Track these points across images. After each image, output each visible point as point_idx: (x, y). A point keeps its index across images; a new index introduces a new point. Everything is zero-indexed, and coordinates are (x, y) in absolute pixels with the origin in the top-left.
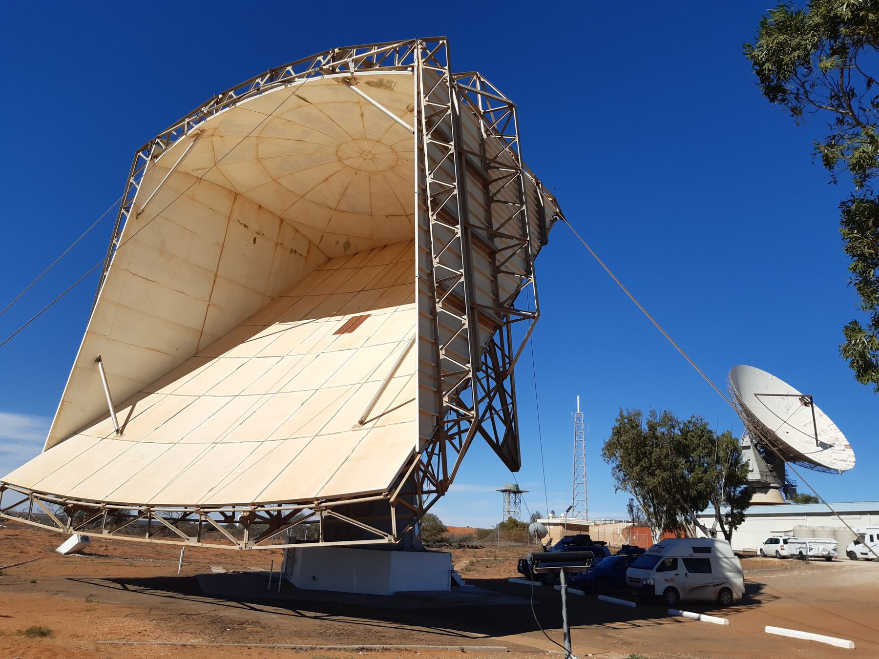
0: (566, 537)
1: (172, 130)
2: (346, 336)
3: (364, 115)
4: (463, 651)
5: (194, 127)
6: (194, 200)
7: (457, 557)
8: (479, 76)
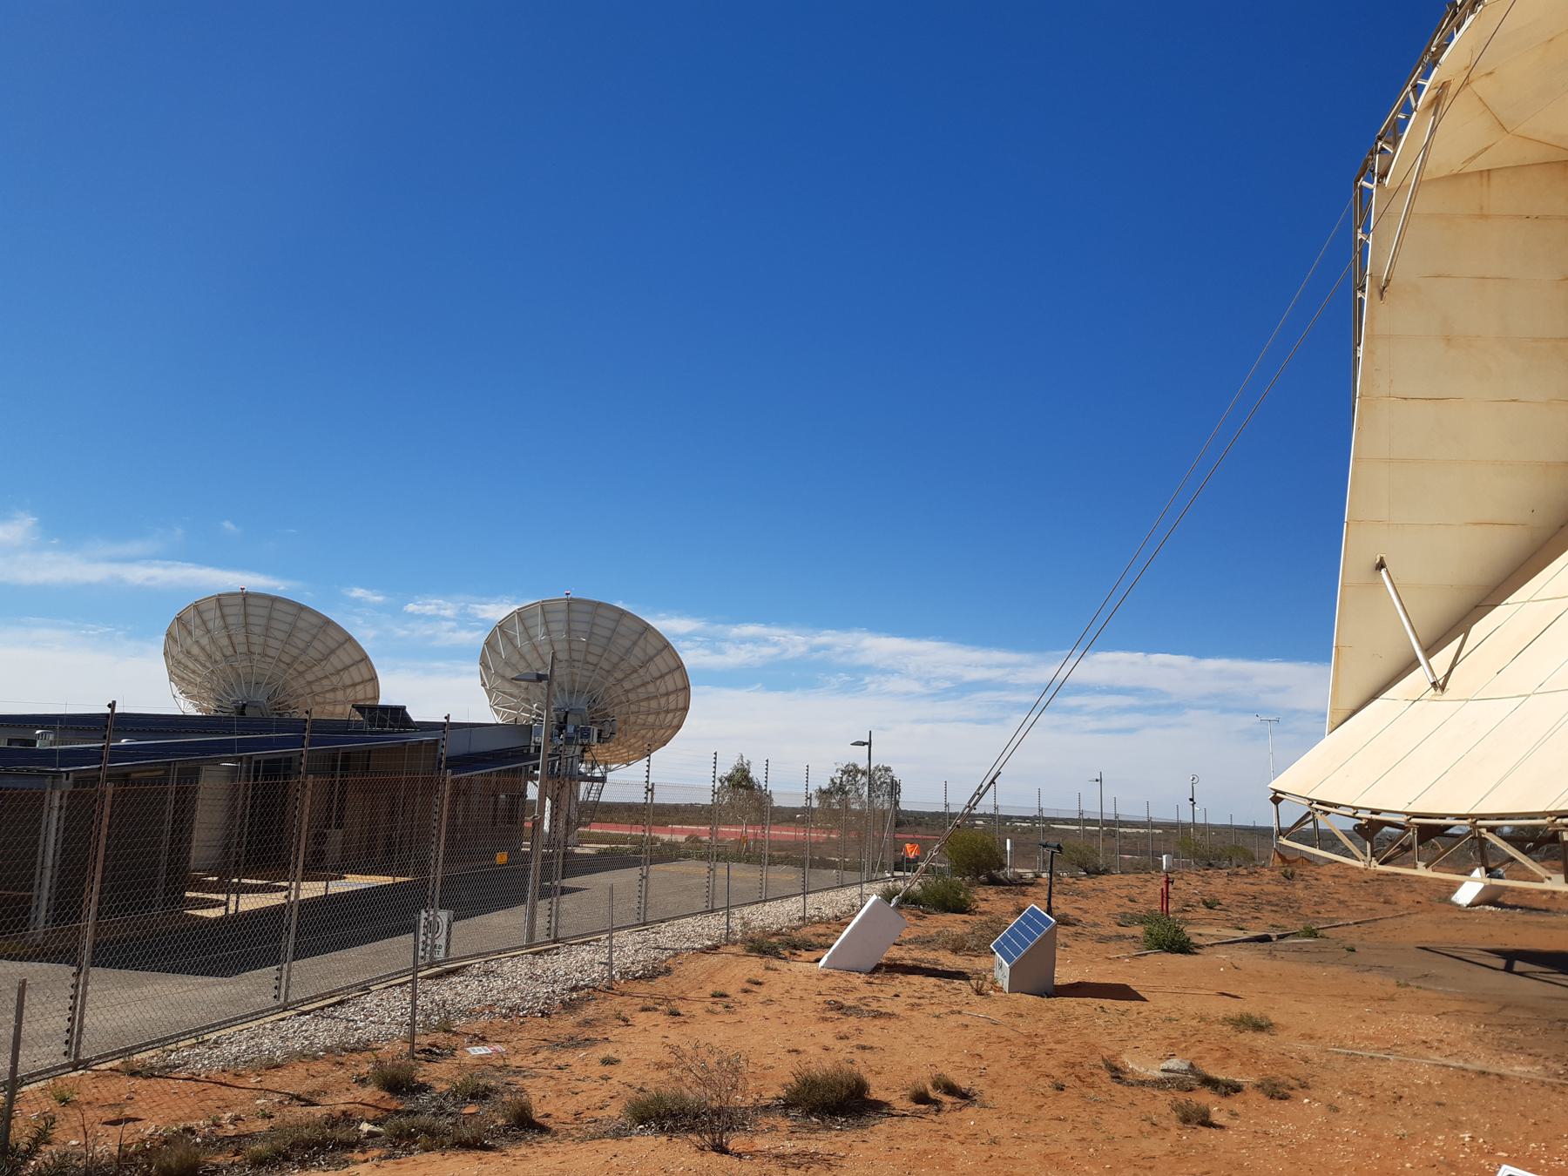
1: (1394, 113)
6: (1483, 216)
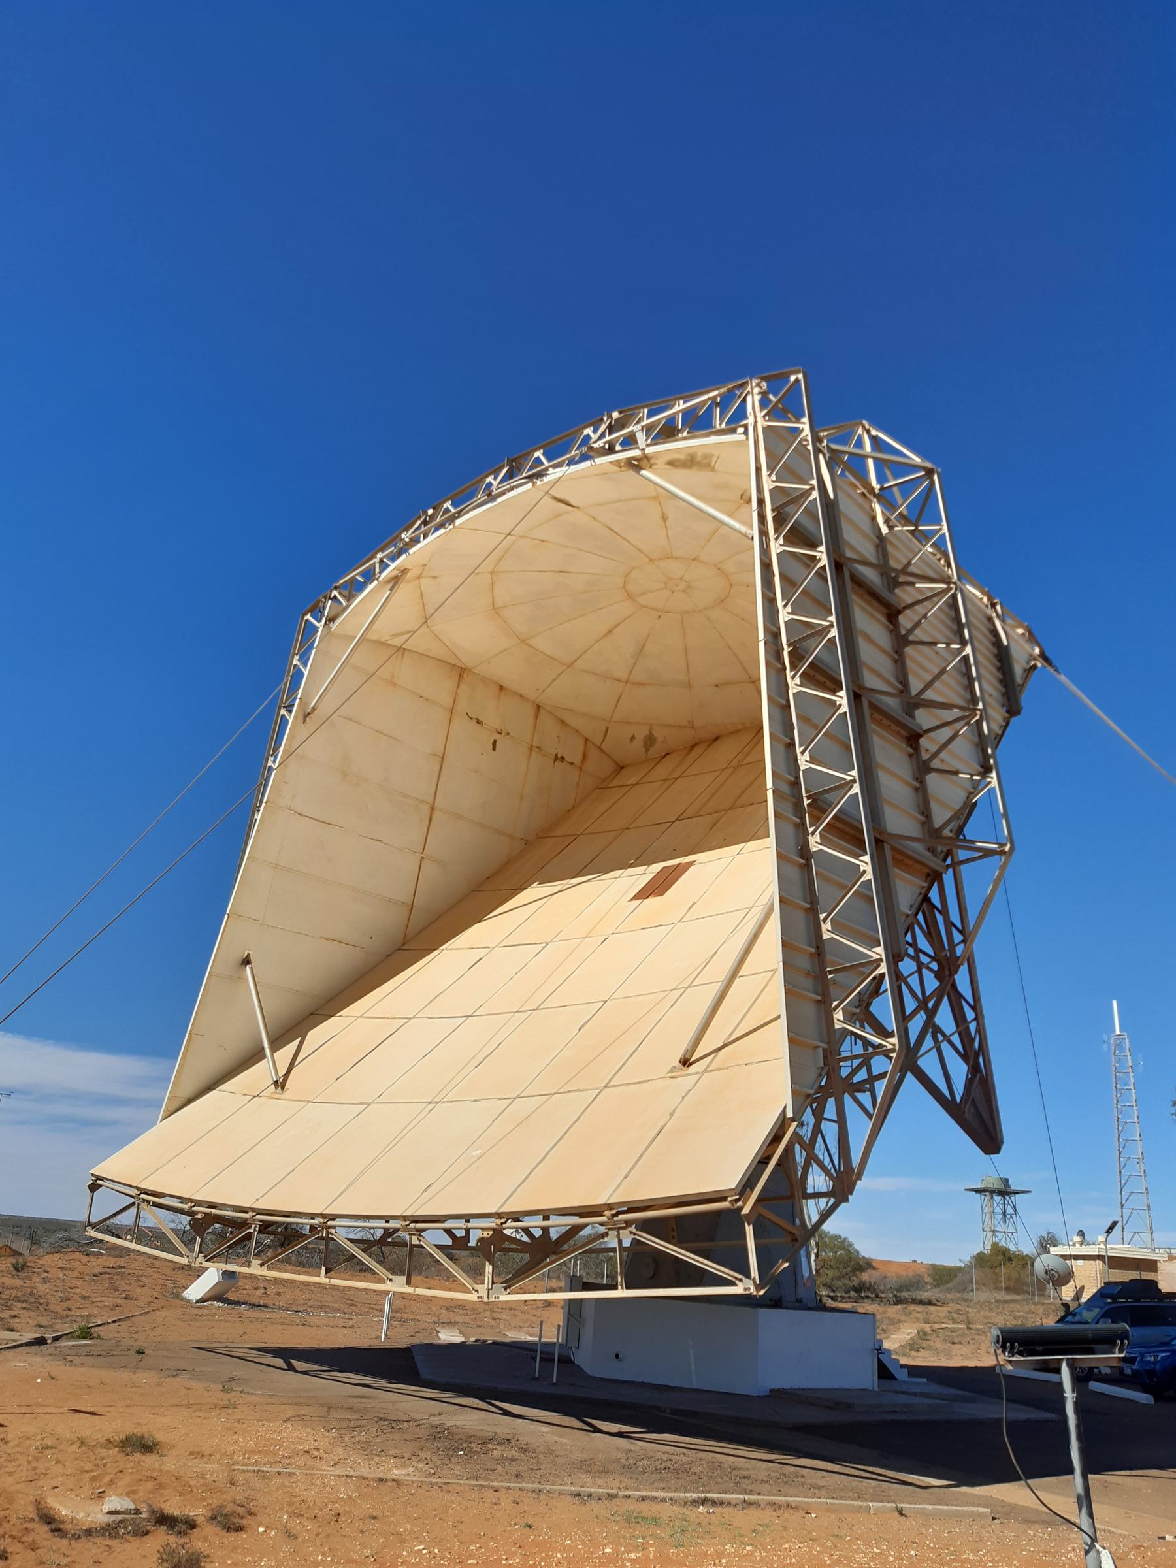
0: (1108, 1284)
1: (356, 574)
2: (653, 901)
3: (668, 518)
4: (901, 1514)
5: (389, 566)
6: (394, 684)
7: (892, 1322)
8: (867, 426)
